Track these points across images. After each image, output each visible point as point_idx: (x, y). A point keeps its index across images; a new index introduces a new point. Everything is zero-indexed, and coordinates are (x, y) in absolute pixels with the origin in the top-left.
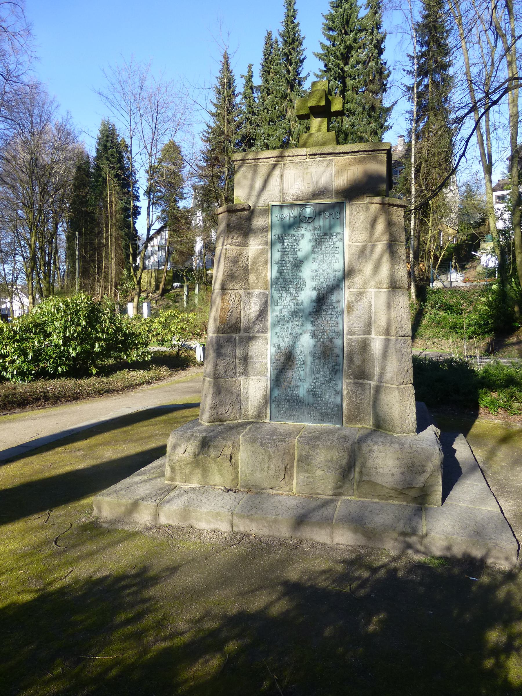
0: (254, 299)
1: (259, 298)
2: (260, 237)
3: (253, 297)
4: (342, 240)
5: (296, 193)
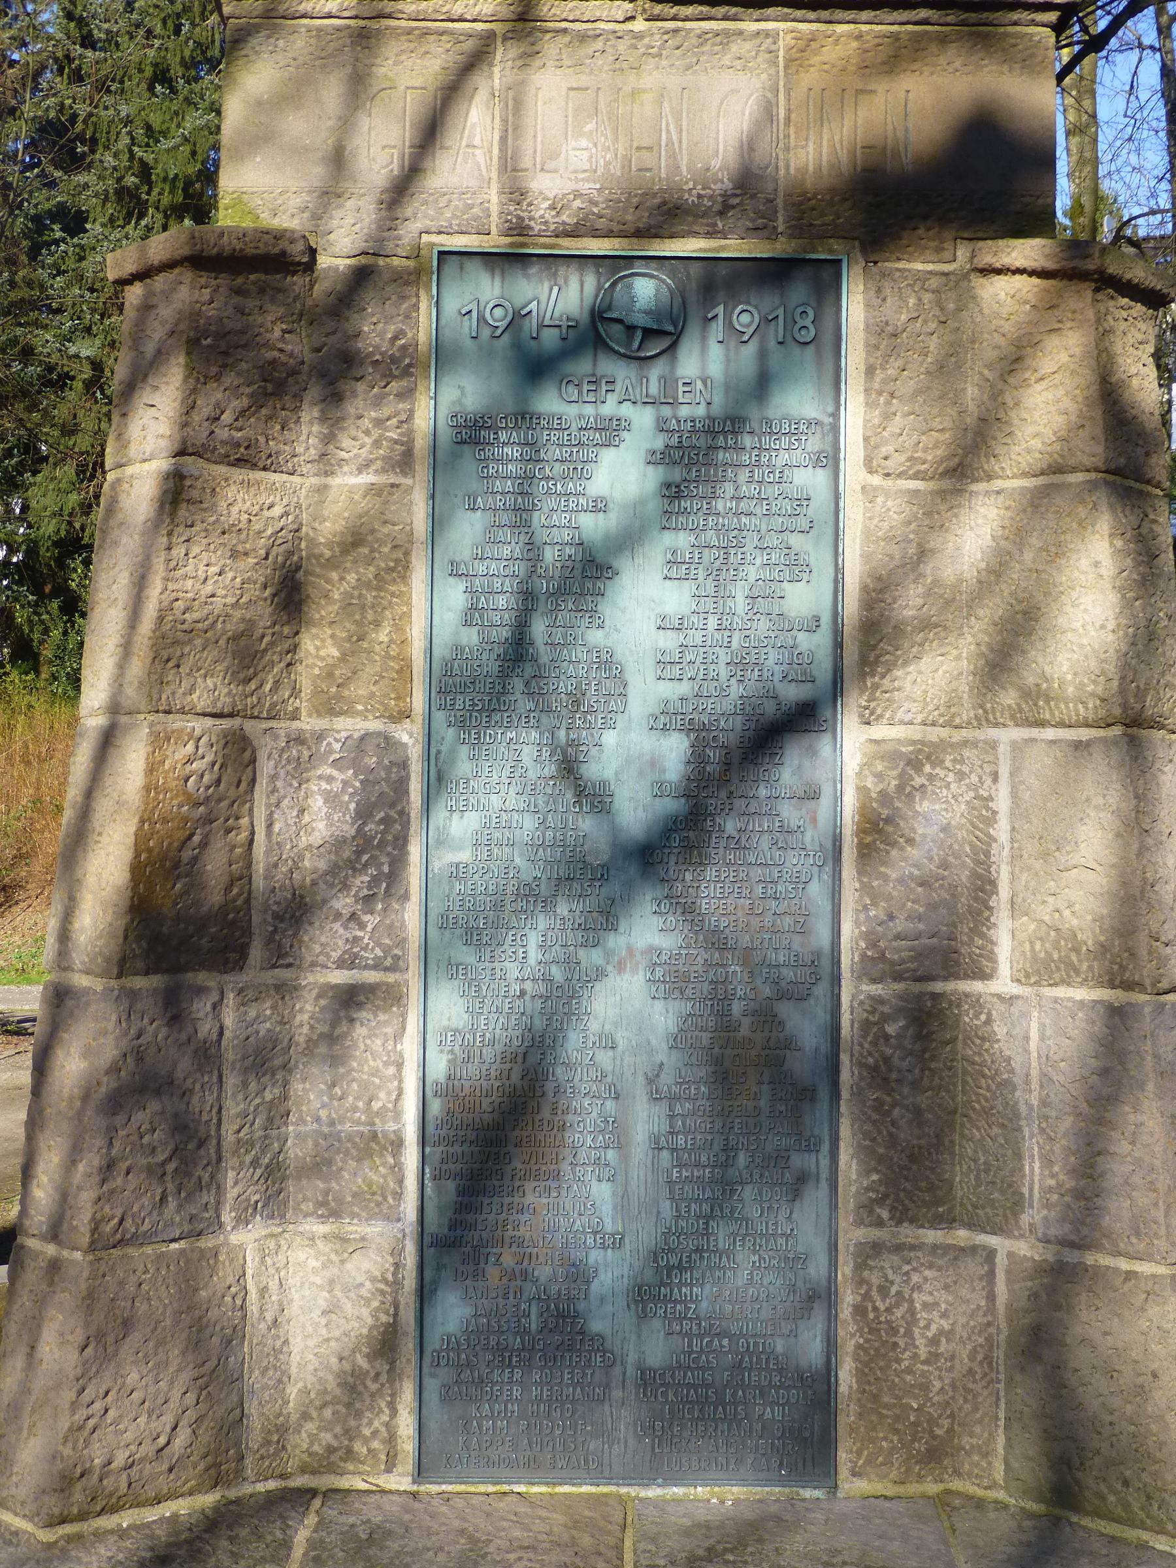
0: (328, 770)
1: (356, 764)
2: (366, 423)
3: (323, 759)
4: (831, 460)
5: (577, 195)
